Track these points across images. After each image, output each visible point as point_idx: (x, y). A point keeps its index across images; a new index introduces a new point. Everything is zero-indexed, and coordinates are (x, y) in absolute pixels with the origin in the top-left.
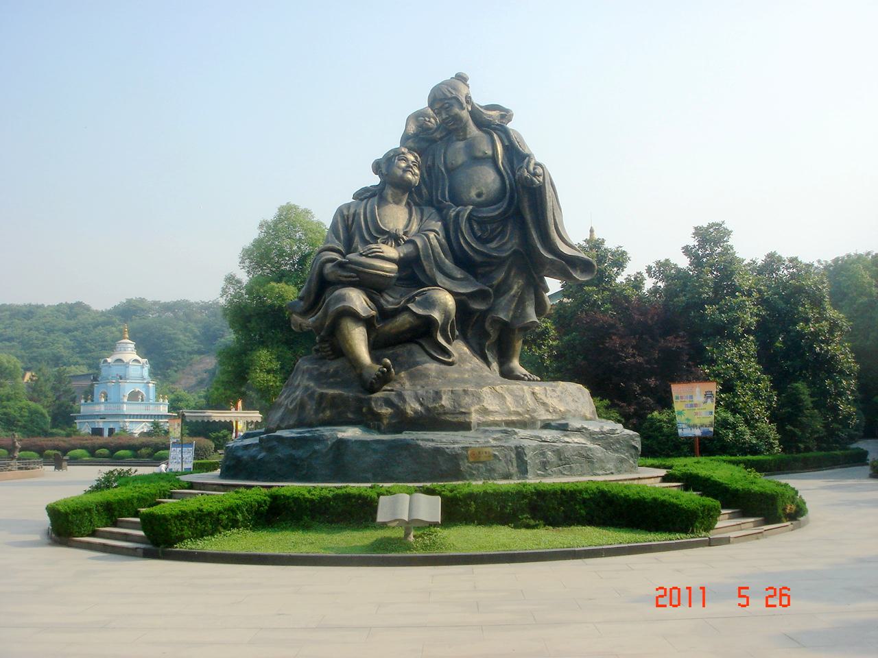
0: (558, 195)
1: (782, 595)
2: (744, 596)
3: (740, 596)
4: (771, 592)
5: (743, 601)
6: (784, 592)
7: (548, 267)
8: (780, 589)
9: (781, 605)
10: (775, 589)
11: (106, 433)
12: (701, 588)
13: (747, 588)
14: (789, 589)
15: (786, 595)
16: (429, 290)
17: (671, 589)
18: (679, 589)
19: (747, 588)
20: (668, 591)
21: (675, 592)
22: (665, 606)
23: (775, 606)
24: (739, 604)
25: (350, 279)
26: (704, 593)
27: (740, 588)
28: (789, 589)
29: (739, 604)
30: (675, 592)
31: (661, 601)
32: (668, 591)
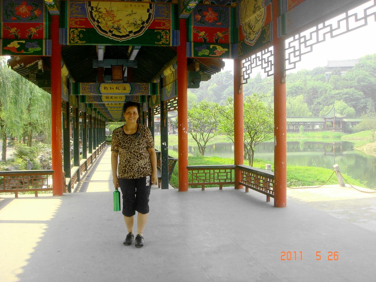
0: (304, 55)
1: (335, 255)
2: (319, 256)
3: (317, 255)
4: (330, 254)
5: (318, 258)
6: (336, 254)
7: (187, 57)
8: (334, 253)
10: (332, 253)
11: (115, 88)
12: (300, 252)
13: (320, 252)
14: (338, 253)
15: (336, 255)
16: (216, 58)
17: (287, 253)
18: (291, 252)
19: (320, 252)
20: (333, 253)
25: (158, 21)
26: (296, 254)
27: (317, 252)
28: (338, 253)
31: (330, 258)
32: (333, 253)
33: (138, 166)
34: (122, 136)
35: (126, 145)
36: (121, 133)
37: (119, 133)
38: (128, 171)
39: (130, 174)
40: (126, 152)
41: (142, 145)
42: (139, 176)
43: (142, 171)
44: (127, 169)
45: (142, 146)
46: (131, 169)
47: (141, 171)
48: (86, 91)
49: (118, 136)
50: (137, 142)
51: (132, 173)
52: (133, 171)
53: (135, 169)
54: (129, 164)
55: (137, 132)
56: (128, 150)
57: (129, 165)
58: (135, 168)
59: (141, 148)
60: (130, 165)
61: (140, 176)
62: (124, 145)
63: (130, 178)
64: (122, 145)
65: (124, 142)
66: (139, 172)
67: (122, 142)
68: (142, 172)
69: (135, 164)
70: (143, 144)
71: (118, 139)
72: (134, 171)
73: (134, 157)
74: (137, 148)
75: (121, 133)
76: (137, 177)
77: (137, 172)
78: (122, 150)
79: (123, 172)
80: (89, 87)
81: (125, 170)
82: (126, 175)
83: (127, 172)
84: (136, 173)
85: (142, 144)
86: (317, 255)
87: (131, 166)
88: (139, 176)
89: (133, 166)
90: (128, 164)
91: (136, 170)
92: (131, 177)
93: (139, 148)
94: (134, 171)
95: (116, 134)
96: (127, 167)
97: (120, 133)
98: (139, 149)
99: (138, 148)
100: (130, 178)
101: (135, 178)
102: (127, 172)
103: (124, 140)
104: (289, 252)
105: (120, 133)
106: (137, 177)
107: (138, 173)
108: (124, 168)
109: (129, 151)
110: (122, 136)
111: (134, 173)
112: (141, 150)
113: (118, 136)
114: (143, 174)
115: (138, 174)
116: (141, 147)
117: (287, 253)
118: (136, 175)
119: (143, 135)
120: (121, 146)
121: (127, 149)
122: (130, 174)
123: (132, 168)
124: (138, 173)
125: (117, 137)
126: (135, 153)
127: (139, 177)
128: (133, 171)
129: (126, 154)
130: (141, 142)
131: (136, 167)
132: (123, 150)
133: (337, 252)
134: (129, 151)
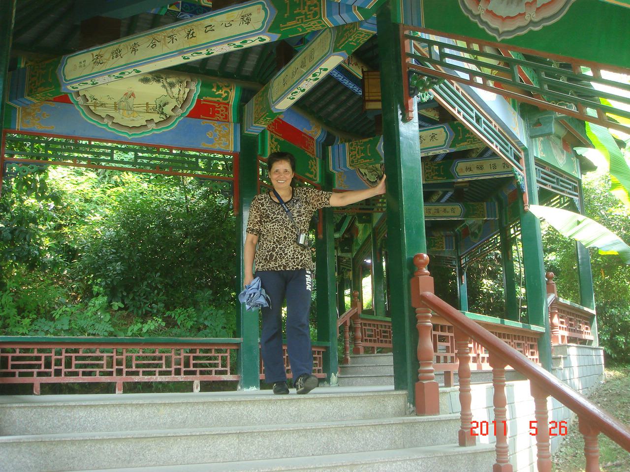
1: (561, 427)
6: (563, 424)
9: (481, 433)
14: (566, 423)
15: (564, 427)
20: (558, 424)
21: (485, 424)
22: (556, 435)
23: (556, 435)
24: (531, 434)
28: (566, 423)
29: (531, 434)
30: (485, 424)
31: (553, 431)
32: (558, 424)
33: (292, 249)
34: (270, 205)
35: (278, 218)
36: (267, 200)
37: (263, 201)
38: (276, 257)
39: (280, 263)
40: (278, 228)
41: (304, 216)
42: (295, 266)
43: (300, 259)
44: (275, 255)
45: (304, 218)
46: (283, 254)
47: (298, 258)
48: (430, 175)
49: (263, 205)
50: (295, 211)
51: (284, 260)
52: (285, 258)
53: (289, 254)
54: (280, 246)
55: (292, 198)
56: (282, 225)
57: (279, 248)
58: (288, 252)
59: (303, 221)
60: (281, 248)
61: (297, 266)
62: (274, 217)
63: (280, 268)
64: (272, 218)
65: (274, 213)
66: (295, 259)
67: (270, 214)
68: (299, 260)
69: (289, 246)
70: (305, 215)
71: (263, 209)
72: (287, 258)
73: (292, 235)
74: (297, 220)
75: (267, 200)
76: (291, 268)
77: (292, 259)
78: (272, 225)
79: (266, 259)
80: (436, 167)
81: (271, 256)
82: (272, 265)
83: (274, 258)
84: (290, 261)
85: (304, 214)
86: (531, 427)
87: (283, 249)
88: (295, 266)
89: (286, 250)
90: (279, 246)
91: (290, 256)
92: (282, 267)
93: (300, 221)
94: (287, 258)
95: (259, 201)
96: (276, 250)
97: (265, 200)
98: (300, 223)
99: (298, 221)
100: (280, 268)
101: (288, 269)
102: (274, 258)
103: (273, 210)
104: (484, 422)
105: (265, 200)
106: (291, 268)
107: (294, 261)
108: (270, 253)
109: (284, 227)
110: (270, 205)
111: (288, 260)
112: (303, 224)
113: (263, 205)
114: (301, 264)
115: (293, 263)
116: (304, 219)
117: (481, 423)
118: (290, 264)
119: (304, 200)
120: (270, 219)
121: (281, 223)
122: (280, 263)
123: (284, 251)
124: (294, 261)
125: (260, 206)
126: (294, 230)
127: (295, 268)
128: (285, 258)
129: (279, 232)
130: (302, 211)
131: (290, 250)
132: (273, 226)
133: (564, 422)
134: (284, 227)
